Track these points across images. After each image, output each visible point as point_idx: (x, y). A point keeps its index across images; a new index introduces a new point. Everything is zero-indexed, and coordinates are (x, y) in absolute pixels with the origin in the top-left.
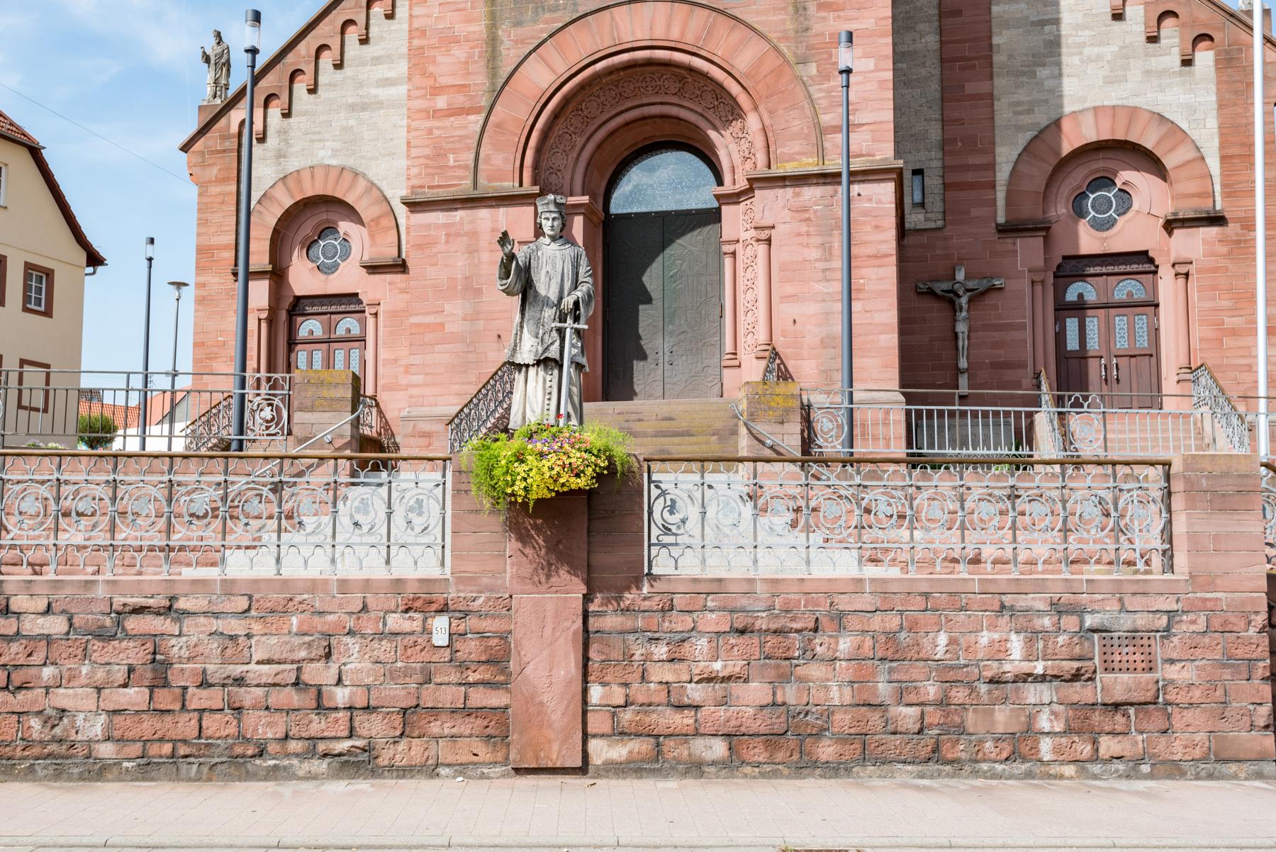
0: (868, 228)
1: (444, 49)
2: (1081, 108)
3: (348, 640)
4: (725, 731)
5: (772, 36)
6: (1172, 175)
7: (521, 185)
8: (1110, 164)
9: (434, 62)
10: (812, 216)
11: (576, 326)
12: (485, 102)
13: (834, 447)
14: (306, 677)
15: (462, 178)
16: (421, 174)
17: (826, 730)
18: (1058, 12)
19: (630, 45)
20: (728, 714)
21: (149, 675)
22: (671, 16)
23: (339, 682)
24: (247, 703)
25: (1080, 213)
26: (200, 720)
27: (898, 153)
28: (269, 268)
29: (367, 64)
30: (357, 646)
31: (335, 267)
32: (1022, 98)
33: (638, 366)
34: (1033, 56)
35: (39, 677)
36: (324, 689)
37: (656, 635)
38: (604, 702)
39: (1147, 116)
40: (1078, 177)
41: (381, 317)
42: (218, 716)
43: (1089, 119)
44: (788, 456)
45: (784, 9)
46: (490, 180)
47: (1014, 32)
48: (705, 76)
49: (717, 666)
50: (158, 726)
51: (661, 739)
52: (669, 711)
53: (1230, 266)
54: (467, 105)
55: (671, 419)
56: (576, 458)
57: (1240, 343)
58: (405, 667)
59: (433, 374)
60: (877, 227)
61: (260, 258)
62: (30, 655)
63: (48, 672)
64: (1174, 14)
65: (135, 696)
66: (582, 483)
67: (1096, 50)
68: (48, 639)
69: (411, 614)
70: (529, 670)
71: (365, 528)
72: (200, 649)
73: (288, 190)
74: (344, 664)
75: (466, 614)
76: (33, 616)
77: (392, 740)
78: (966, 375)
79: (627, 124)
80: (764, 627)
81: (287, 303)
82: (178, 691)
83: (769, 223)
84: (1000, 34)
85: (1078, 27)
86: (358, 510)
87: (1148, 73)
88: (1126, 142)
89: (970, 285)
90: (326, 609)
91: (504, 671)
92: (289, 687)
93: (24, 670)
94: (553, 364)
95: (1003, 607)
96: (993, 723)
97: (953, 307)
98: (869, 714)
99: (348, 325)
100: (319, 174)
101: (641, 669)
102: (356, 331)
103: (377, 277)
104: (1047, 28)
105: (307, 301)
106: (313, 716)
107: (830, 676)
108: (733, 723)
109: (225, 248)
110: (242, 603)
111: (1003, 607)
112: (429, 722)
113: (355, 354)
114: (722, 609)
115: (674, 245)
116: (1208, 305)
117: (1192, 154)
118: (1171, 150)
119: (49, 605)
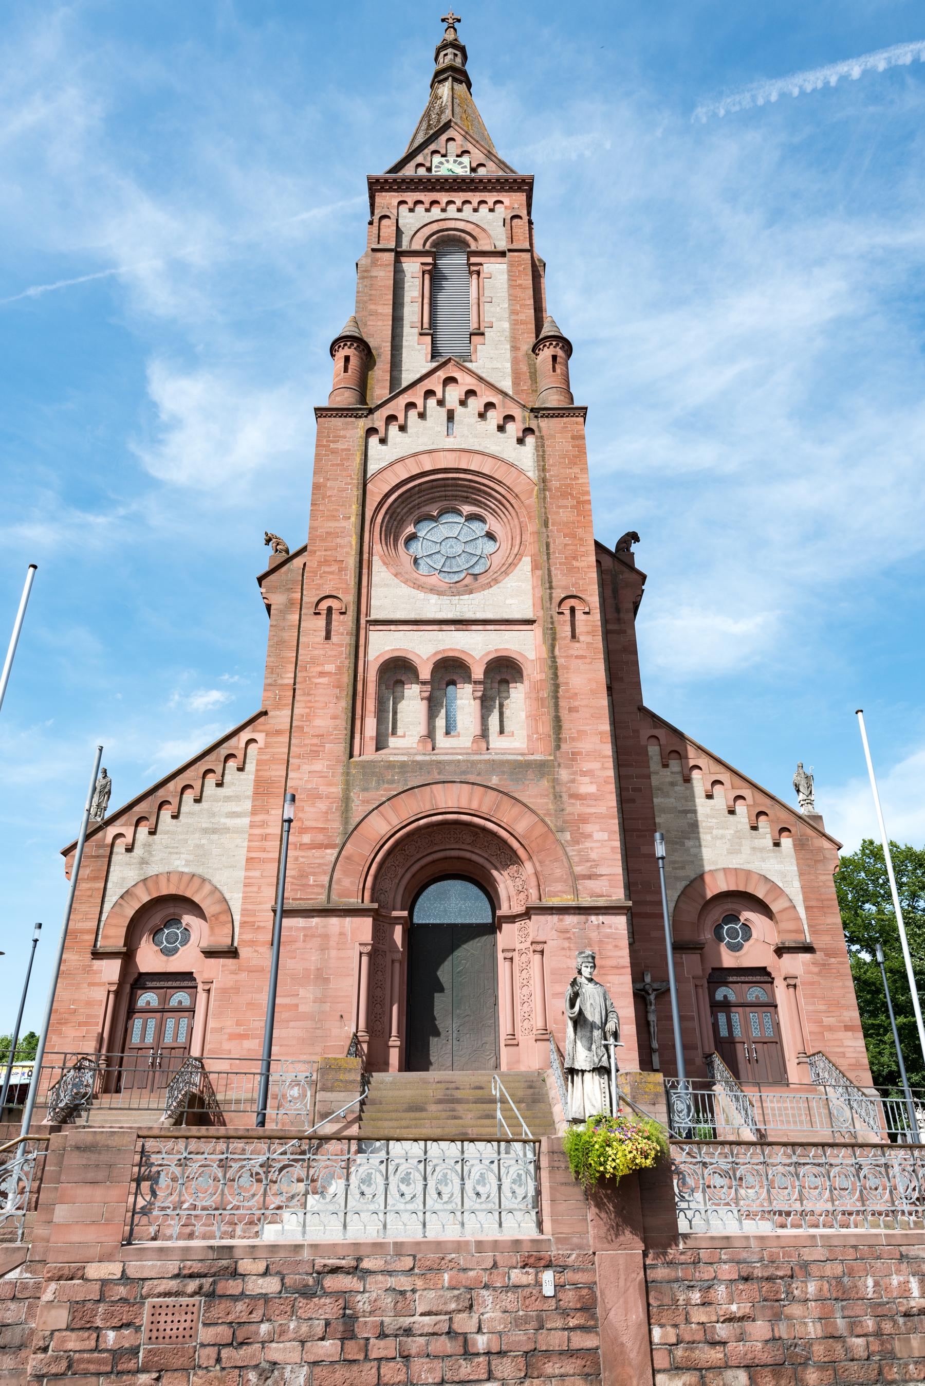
0: (610, 947)
3: (484, 1293)
4: (744, 1363)
5: (539, 812)
6: (778, 916)
7: (363, 902)
8: (736, 906)
12: (338, 841)
13: (686, 1123)
14: (455, 1326)
17: (810, 1359)
18: (695, 806)
19: (444, 810)
20: (746, 1349)
21: (341, 1328)
22: (471, 793)
23: (479, 1330)
24: (413, 1351)
25: (720, 939)
26: (379, 1369)
27: (629, 896)
28: (124, 950)
30: (491, 1297)
31: (176, 950)
32: (677, 859)
33: (433, 1041)
35: (257, 1333)
36: (469, 1336)
37: (692, 1283)
38: (663, 1341)
39: (756, 877)
40: (717, 914)
41: (212, 993)
42: (392, 1364)
43: (721, 876)
45: (547, 795)
46: (340, 896)
47: (669, 816)
48: (494, 834)
49: (734, 1308)
50: (347, 1375)
51: (704, 1371)
52: (706, 1348)
53: (822, 981)
54: (326, 842)
55: (481, 1088)
56: (643, 1144)
57: (835, 1037)
58: (525, 1315)
59: (286, 1045)
60: (616, 946)
61: (114, 939)
62: (251, 1313)
63: (264, 1328)
64: (766, 814)
65: (329, 1348)
66: (649, 1162)
67: (721, 832)
68: (265, 1298)
69: (527, 1269)
70: (612, 1315)
71: (484, 1197)
72: (378, 1303)
73: (147, 889)
74: (482, 1314)
75: (565, 1268)
76: (255, 1277)
77: (519, 1381)
78: (657, 1054)
79: (434, 861)
80: (760, 1275)
81: (131, 980)
82: (362, 1342)
83: (543, 940)
85: (707, 816)
86: (478, 1182)
88: (746, 893)
89: (655, 986)
90: (469, 1266)
91: (593, 1317)
92: (444, 1336)
93: (246, 1327)
95: (902, 1255)
96: (911, 1349)
98: (835, 1345)
99: (180, 998)
100: (174, 879)
101: (684, 1312)
102: (187, 1003)
103: (212, 961)
104: (689, 815)
105: (147, 977)
106: (461, 1361)
107: (806, 1314)
108: (750, 1356)
109: (88, 932)
110: (408, 1262)
111: (902, 1255)
112: (545, 1363)
113: (184, 1023)
114: (731, 1261)
115: (461, 949)
116: (811, 1008)
117: (787, 904)
118: (775, 900)
119: (267, 1266)
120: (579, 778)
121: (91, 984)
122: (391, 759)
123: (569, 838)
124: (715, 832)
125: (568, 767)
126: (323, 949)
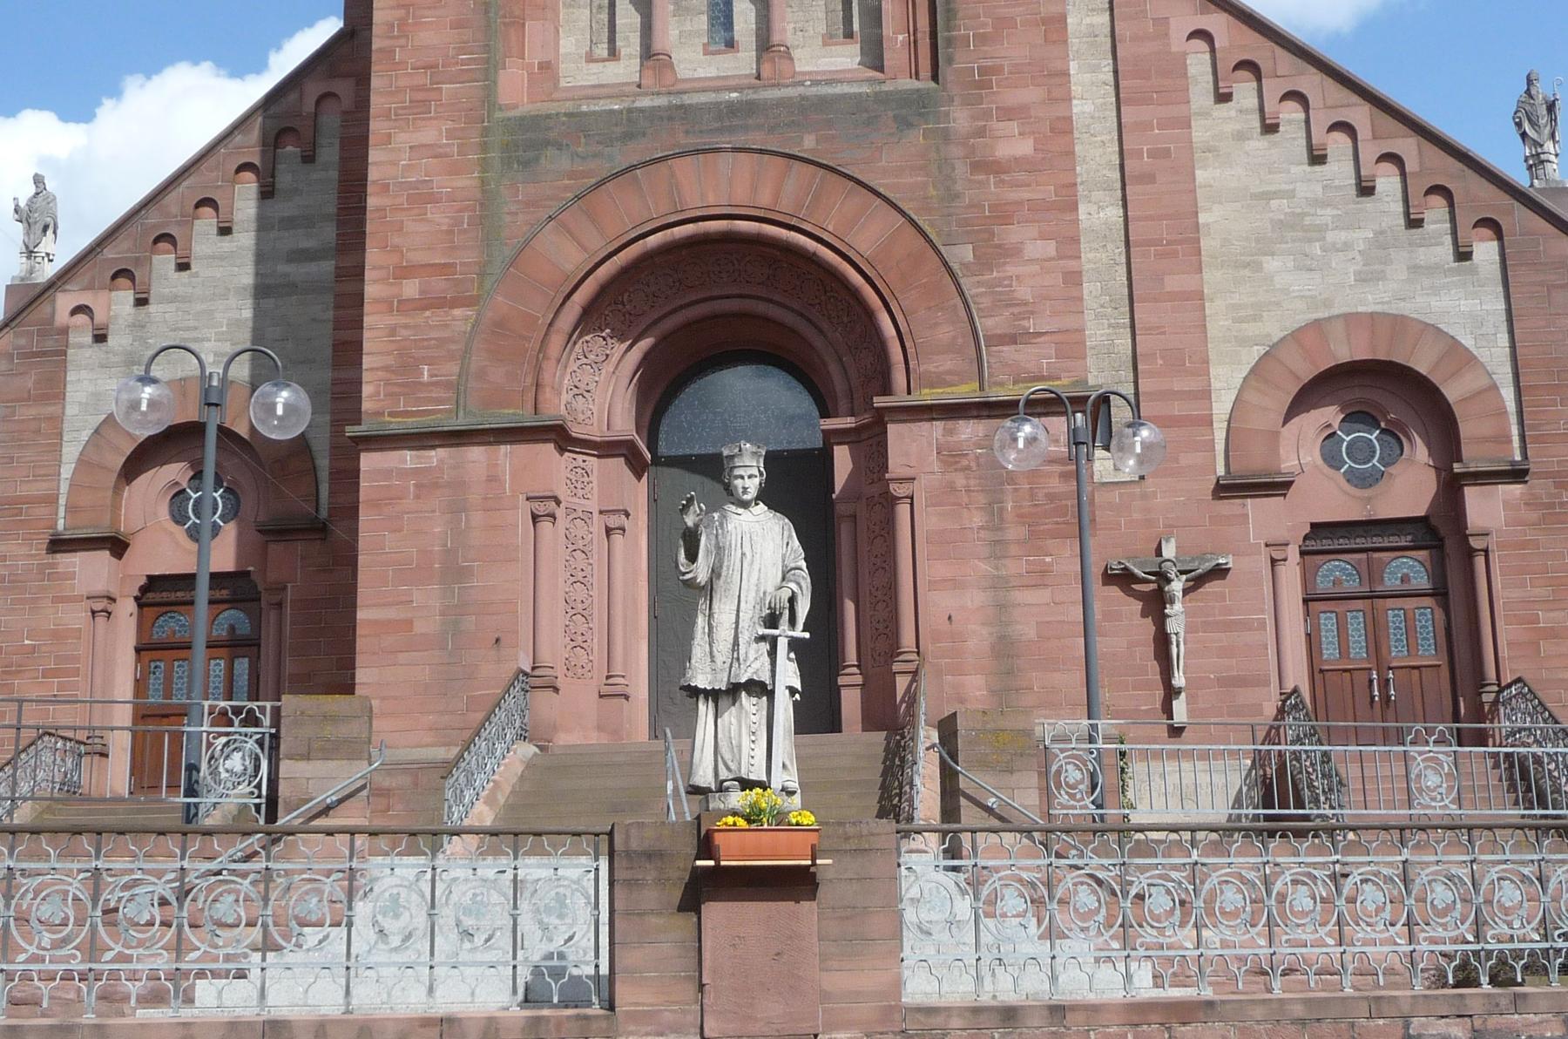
1: (416, 211)
2: (1326, 315)
9: (401, 229)
10: (973, 464)
11: (791, 633)
13: (1086, 807)
15: (440, 401)
16: (378, 394)
19: (699, 213)
29: (273, 227)
34: (1258, 241)
44: (1016, 824)
67: (1343, 236)
84: (1210, 210)
87: (1414, 269)
94: (758, 689)
97: (1156, 604)
102: (244, 628)
120: (994, 124)
121: (57, 600)
122: (584, 108)
123: (970, 257)
124: (1331, 236)
125: (967, 102)
126: (457, 509)
